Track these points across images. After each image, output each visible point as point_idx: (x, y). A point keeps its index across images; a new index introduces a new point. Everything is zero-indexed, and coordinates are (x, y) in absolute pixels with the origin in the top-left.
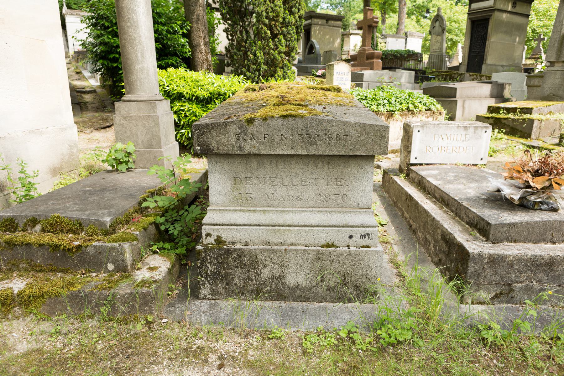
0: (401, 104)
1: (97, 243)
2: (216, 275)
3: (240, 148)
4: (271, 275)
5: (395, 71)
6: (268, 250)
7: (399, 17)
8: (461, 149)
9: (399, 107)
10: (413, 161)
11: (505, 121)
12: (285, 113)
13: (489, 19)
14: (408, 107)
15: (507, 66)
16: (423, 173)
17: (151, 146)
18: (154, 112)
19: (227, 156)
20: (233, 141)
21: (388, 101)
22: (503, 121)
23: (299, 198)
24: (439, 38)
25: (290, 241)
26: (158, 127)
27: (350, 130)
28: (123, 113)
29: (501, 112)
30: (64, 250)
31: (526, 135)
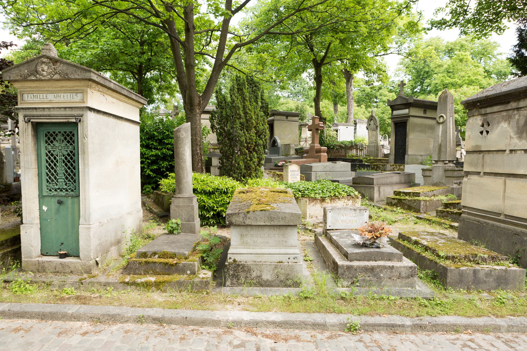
0: (330, 192)
1: (183, 262)
2: (233, 275)
3: (244, 222)
4: (256, 275)
5: (336, 163)
6: (255, 264)
7: (348, 108)
8: (354, 221)
9: (328, 194)
10: (328, 228)
11: (403, 201)
12: (261, 209)
13: (406, 122)
14: (335, 194)
15: (425, 155)
16: (331, 234)
17: (189, 221)
18: (192, 203)
19: (239, 225)
20: (241, 220)
21: (322, 191)
22: (403, 201)
23: (267, 243)
24: (374, 132)
25: (264, 261)
26: (193, 211)
27: (286, 215)
28: (176, 204)
29: (401, 195)
30: (170, 265)
31: (418, 211)
